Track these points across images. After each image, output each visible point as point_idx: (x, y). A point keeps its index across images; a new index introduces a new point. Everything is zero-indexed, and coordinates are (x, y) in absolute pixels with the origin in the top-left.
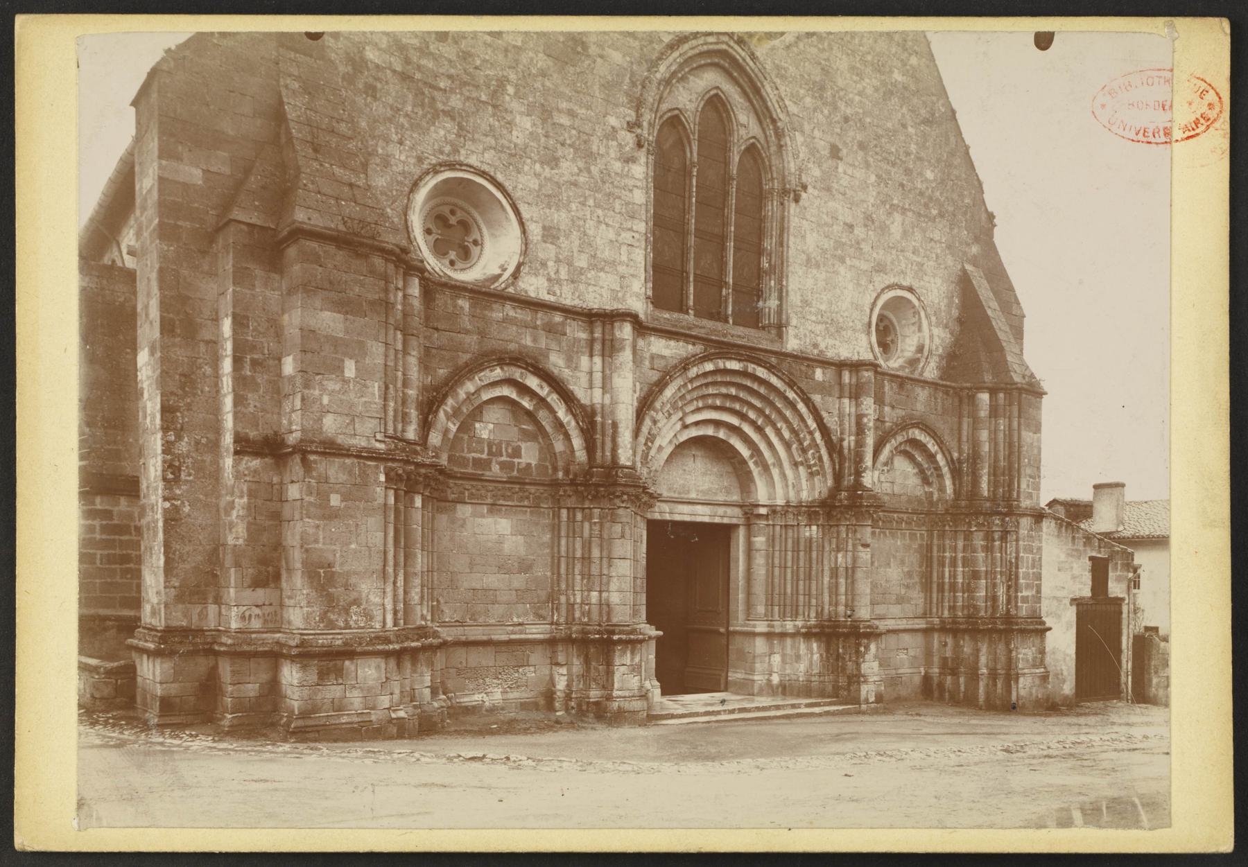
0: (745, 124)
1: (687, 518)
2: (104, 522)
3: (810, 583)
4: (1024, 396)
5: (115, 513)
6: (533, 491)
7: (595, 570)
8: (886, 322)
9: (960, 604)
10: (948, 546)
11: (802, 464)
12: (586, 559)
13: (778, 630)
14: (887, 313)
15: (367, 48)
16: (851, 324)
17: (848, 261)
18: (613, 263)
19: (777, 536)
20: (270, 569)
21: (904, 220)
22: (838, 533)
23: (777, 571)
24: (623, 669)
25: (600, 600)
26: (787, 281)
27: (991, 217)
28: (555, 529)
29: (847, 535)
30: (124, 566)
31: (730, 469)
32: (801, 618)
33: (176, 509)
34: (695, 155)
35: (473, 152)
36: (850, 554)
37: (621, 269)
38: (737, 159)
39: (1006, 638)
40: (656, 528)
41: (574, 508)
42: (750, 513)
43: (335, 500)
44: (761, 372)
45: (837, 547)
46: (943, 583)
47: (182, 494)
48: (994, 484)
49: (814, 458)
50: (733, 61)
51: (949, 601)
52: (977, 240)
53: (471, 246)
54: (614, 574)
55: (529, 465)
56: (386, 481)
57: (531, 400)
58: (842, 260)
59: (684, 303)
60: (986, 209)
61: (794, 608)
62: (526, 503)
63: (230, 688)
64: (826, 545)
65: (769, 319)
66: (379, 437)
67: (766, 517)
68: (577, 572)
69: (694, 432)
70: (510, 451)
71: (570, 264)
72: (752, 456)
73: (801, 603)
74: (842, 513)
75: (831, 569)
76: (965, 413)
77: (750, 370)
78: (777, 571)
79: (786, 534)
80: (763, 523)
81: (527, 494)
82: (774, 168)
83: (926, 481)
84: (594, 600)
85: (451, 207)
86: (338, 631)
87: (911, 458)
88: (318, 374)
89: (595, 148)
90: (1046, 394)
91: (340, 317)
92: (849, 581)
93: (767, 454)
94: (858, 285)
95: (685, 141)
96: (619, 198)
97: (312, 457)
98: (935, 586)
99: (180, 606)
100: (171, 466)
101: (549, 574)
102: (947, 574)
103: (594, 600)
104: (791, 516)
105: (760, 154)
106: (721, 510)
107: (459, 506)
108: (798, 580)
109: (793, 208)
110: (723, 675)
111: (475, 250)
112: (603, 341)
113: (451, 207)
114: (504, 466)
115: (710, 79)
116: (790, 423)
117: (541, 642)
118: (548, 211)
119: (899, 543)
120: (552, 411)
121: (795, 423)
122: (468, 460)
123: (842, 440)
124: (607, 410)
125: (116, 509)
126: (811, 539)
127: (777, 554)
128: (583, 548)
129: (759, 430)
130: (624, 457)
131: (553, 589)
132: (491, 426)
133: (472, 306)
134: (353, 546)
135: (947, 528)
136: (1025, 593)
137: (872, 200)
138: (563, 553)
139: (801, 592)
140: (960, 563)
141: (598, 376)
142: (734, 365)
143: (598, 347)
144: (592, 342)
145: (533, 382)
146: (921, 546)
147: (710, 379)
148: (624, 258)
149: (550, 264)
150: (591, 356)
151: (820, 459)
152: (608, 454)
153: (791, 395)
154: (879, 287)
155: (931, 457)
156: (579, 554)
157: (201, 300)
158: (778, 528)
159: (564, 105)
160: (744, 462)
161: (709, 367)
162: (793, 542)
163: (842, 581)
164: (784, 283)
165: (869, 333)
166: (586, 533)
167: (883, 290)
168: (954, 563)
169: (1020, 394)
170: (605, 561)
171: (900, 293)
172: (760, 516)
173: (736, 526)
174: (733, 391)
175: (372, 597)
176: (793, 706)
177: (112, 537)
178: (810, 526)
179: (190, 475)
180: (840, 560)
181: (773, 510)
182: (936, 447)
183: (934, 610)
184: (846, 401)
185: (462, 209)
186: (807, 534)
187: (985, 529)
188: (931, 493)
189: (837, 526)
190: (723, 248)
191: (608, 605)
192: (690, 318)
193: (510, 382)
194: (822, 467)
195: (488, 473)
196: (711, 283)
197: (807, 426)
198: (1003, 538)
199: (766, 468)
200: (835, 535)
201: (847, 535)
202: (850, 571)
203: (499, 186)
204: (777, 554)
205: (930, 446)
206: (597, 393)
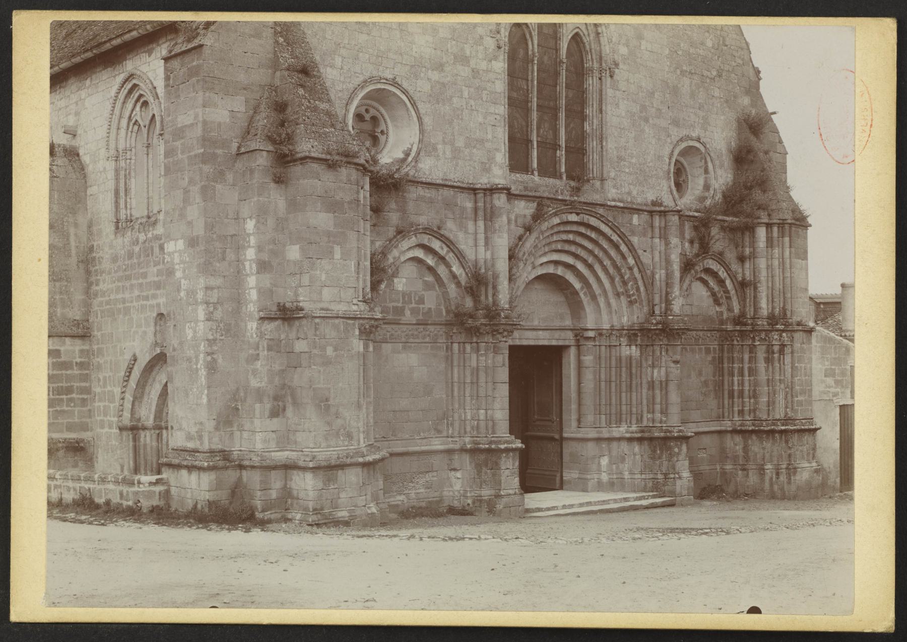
1: (532, 343)
2: (54, 360)
3: (631, 395)
4: (793, 229)
5: (62, 352)
6: (433, 330)
8: (679, 166)
9: (746, 408)
10: (736, 359)
11: (623, 294)
13: (606, 435)
14: (682, 160)
16: (655, 172)
17: (651, 121)
18: (482, 141)
19: (603, 355)
20: (280, 403)
21: (691, 83)
22: (653, 351)
23: (603, 384)
24: (507, 472)
25: (486, 417)
26: (607, 141)
27: (757, 72)
28: (449, 359)
29: (661, 353)
30: (69, 396)
31: (563, 299)
32: (624, 424)
33: (214, 360)
34: (536, 46)
35: (387, 68)
36: (663, 369)
37: (488, 145)
38: (566, 46)
39: (785, 437)
40: (516, 352)
41: (464, 343)
42: (580, 335)
43: (330, 351)
44: (593, 221)
45: (653, 363)
46: (733, 390)
47: (217, 350)
48: (771, 300)
49: (632, 289)
51: (738, 406)
52: (748, 92)
53: (379, 135)
54: (497, 395)
55: (430, 309)
56: (359, 335)
57: (433, 259)
58: (646, 120)
59: (530, 166)
60: (753, 65)
61: (618, 417)
63: (259, 493)
64: (644, 362)
65: (593, 174)
66: (355, 301)
67: (594, 339)
68: (467, 394)
69: (540, 271)
70: (417, 299)
71: (453, 144)
72: (582, 288)
73: (624, 412)
74: (657, 335)
75: (648, 382)
76: (747, 244)
77: (585, 220)
78: (603, 384)
79: (610, 352)
80: (590, 344)
81: (428, 333)
82: (593, 51)
83: (717, 302)
84: (482, 417)
85: (366, 107)
86: (332, 449)
87: (705, 282)
88: (318, 259)
89: (468, 53)
90: (810, 226)
91: (331, 215)
92: (664, 392)
93: (595, 286)
94: (659, 139)
95: (528, 36)
96: (485, 89)
98: (726, 393)
99: (218, 433)
101: (444, 396)
102: (736, 383)
103: (482, 417)
104: (614, 338)
105: (581, 39)
106: (557, 334)
107: (384, 345)
108: (621, 392)
110: (559, 475)
111: (382, 138)
112: (485, 210)
113: (366, 107)
114: (414, 311)
116: (614, 261)
117: (442, 452)
118: (437, 106)
119: (697, 357)
120: (448, 266)
121: (618, 259)
122: (390, 308)
123: (653, 274)
124: (489, 264)
125: (62, 349)
126: (631, 357)
127: (603, 370)
128: (472, 374)
129: (590, 267)
130: (503, 298)
131: (448, 409)
132: (404, 280)
134: (340, 385)
135: (735, 342)
136: (800, 398)
137: (667, 69)
138: (456, 379)
139: (624, 402)
140: (746, 373)
141: (481, 237)
142: (573, 218)
143: (481, 213)
144: (476, 210)
145: (436, 245)
146: (714, 358)
147: (556, 230)
148: (490, 136)
149: (440, 147)
150: (476, 221)
151: (638, 289)
152: (490, 299)
153: (615, 238)
154: (675, 139)
155: (721, 282)
156: (468, 380)
158: (603, 348)
160: (576, 293)
162: (616, 359)
163: (658, 392)
164: (604, 144)
165: (669, 178)
166: (474, 364)
168: (741, 374)
169: (790, 227)
170: (490, 384)
171: (691, 143)
172: (588, 338)
173: (568, 347)
174: (571, 237)
175: (352, 422)
176: (626, 500)
177: (60, 372)
178: (630, 345)
179: (222, 336)
180: (655, 374)
181: (600, 333)
182: (725, 274)
183: (726, 414)
184: (657, 240)
185: (374, 108)
186: (628, 353)
187: (767, 343)
188: (722, 313)
189: (652, 345)
190: (556, 118)
191: (493, 421)
192: (536, 178)
194: (639, 296)
195: (404, 318)
196: (549, 147)
197: (627, 263)
198: (782, 352)
199: (594, 297)
200: (651, 354)
201: (661, 353)
202: (664, 384)
203: (405, 92)
204: (603, 370)
205: (720, 273)
206: (481, 249)
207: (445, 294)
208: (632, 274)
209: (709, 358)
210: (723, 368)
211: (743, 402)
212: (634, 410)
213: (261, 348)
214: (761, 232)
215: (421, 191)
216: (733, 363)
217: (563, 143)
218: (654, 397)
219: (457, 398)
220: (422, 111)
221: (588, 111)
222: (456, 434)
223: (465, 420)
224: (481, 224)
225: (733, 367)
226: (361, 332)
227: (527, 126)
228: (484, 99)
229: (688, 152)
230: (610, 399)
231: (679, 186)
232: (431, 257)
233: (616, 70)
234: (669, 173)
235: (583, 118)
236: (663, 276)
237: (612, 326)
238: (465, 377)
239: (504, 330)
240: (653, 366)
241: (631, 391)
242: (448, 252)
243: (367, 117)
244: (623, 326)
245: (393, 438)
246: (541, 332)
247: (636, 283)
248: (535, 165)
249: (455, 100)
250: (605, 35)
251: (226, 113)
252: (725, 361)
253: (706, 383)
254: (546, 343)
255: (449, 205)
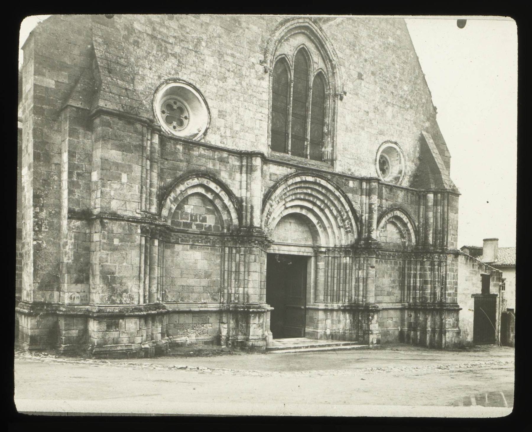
0: (316, 60)
1: (286, 253)
7: (241, 277)
11: (342, 227)
12: (238, 272)
13: (330, 308)
14: (384, 154)
15: (135, 23)
17: (366, 129)
18: (252, 129)
19: (330, 262)
22: (360, 261)
24: (254, 326)
27: (435, 109)
31: (307, 229)
32: (341, 302)
36: (365, 271)
37: (256, 132)
38: (313, 79)
40: (271, 257)
44: (323, 182)
50: (312, 32)
56: (141, 233)
58: (363, 129)
62: (209, 244)
67: (325, 253)
70: (201, 219)
72: (318, 223)
74: (362, 251)
83: (402, 236)
85: (174, 100)
88: (109, 180)
95: (288, 69)
96: (255, 97)
97: (105, 221)
98: (406, 287)
100: (37, 224)
102: (412, 282)
104: (337, 252)
106: (303, 249)
107: (176, 246)
108: (340, 283)
109: (339, 102)
111: (185, 122)
114: (198, 226)
115: (300, 40)
118: (221, 103)
121: (340, 207)
123: (362, 216)
124: (248, 200)
126: (346, 263)
127: (330, 271)
129: (322, 210)
133: (184, 148)
135: (412, 259)
138: (226, 269)
139: (341, 289)
140: (418, 276)
143: (244, 169)
145: (213, 186)
146: (399, 268)
147: (298, 186)
148: (258, 126)
150: (241, 173)
151: (351, 225)
153: (337, 193)
155: (405, 225)
156: (234, 269)
157: (53, 144)
158: (330, 258)
159: (229, 52)
160: (314, 226)
161: (298, 179)
164: (335, 139)
166: (237, 259)
167: (382, 143)
170: (246, 273)
172: (322, 252)
173: (310, 257)
174: (309, 191)
179: (46, 228)
180: (360, 274)
181: (328, 249)
182: (407, 220)
183: (406, 299)
185: (180, 101)
188: (405, 242)
191: (248, 294)
193: (202, 185)
194: (352, 228)
195: (190, 230)
196: (299, 139)
197: (345, 209)
198: (439, 265)
199: (325, 229)
204: (330, 271)
206: (244, 191)
207: (221, 217)
208: (348, 215)
209: (397, 268)
210: (405, 273)
211: (416, 293)
212: (347, 294)
213: (69, 237)
214: (431, 196)
215: (202, 151)
216: (411, 271)
217: (309, 137)
218: (359, 286)
219: (226, 280)
220: (210, 105)
221: (326, 120)
222: (225, 301)
223: (231, 294)
224: (244, 175)
225: (410, 273)
226: (142, 232)
227: (286, 125)
228: (255, 103)
229: (389, 151)
230: (333, 287)
231: (383, 171)
232: (210, 194)
233: (344, 96)
234: (376, 160)
235: (323, 124)
236: (367, 218)
237: (335, 245)
238: (231, 267)
239: (256, 240)
240: (359, 269)
241: (346, 283)
242: (221, 191)
243: (175, 107)
244: (342, 246)
245: (181, 302)
246: (292, 247)
247: (350, 221)
248: (290, 148)
249: (233, 101)
250: (338, 74)
251: (54, 82)
252: (406, 269)
253: (394, 282)
254: (296, 253)
255: (222, 160)
